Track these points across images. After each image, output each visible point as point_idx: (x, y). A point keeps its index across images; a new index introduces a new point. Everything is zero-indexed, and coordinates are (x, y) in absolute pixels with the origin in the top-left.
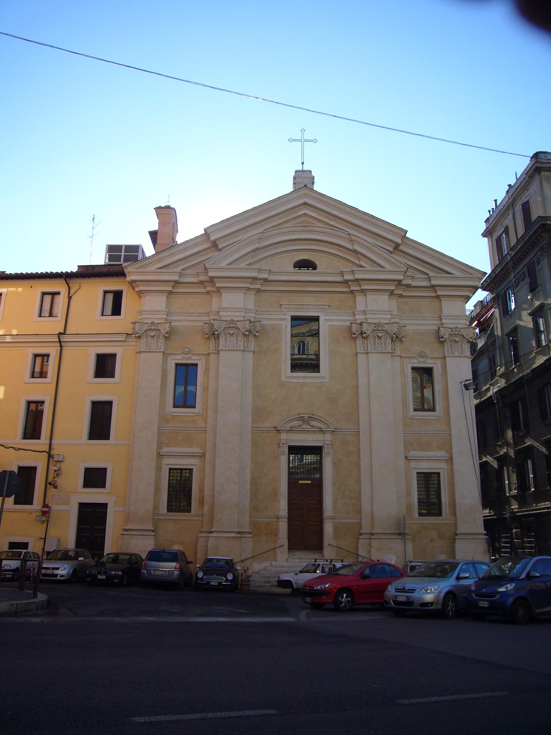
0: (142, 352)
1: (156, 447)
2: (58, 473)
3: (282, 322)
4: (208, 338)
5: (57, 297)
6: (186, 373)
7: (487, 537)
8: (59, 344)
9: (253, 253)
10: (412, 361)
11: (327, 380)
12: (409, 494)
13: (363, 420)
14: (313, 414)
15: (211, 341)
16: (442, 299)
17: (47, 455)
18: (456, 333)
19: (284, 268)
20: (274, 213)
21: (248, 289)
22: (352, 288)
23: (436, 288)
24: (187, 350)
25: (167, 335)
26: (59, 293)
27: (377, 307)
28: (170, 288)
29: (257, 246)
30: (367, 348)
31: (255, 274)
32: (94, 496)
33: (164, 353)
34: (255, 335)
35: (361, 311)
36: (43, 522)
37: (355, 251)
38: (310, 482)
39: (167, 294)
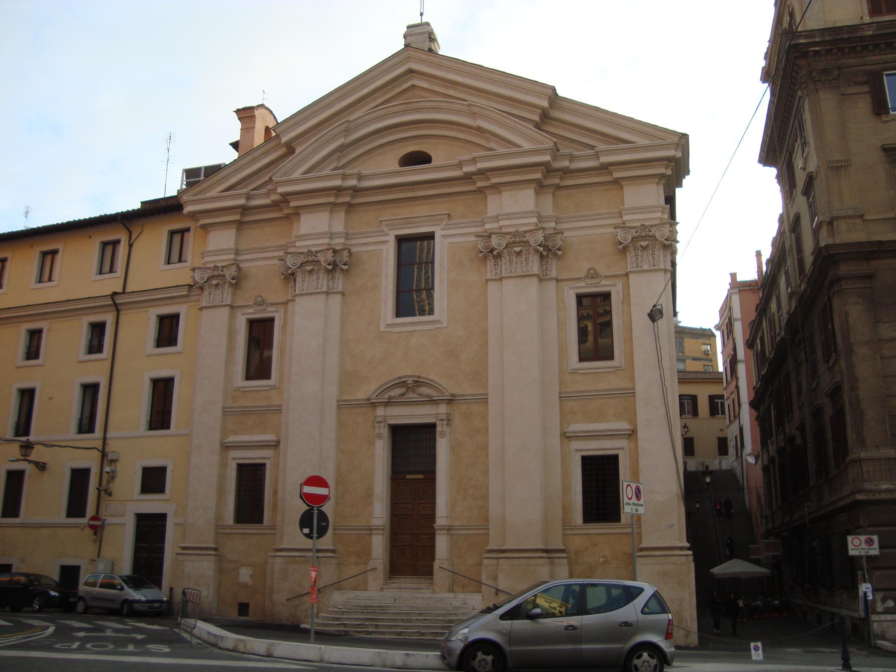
0: (505, 278)
1: (557, 418)
2: (112, 476)
3: (383, 247)
4: (485, 258)
5: (186, 235)
6: (260, 334)
7: (690, 552)
8: (114, 308)
9: (338, 154)
10: (577, 285)
11: (445, 325)
12: (566, 490)
13: (493, 379)
14: (419, 377)
15: (488, 263)
16: (622, 183)
17: (100, 454)
18: (643, 234)
19: (385, 167)
20: (366, 91)
21: (334, 205)
22: (477, 185)
23: (610, 168)
24: (259, 299)
25: (234, 282)
26: (188, 230)
27: (516, 208)
28: (237, 217)
29: (341, 141)
30: (501, 271)
31: (337, 183)
32: (152, 504)
33: (232, 307)
34: (342, 270)
35: (492, 218)
36: (95, 541)
37: (480, 130)
38: (422, 476)
39: (344, 208)
